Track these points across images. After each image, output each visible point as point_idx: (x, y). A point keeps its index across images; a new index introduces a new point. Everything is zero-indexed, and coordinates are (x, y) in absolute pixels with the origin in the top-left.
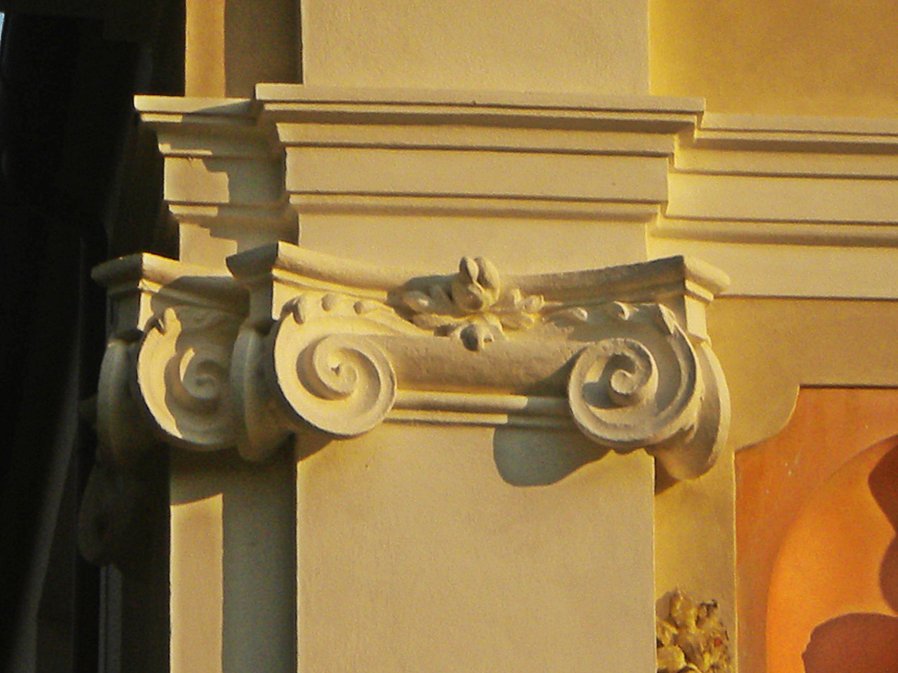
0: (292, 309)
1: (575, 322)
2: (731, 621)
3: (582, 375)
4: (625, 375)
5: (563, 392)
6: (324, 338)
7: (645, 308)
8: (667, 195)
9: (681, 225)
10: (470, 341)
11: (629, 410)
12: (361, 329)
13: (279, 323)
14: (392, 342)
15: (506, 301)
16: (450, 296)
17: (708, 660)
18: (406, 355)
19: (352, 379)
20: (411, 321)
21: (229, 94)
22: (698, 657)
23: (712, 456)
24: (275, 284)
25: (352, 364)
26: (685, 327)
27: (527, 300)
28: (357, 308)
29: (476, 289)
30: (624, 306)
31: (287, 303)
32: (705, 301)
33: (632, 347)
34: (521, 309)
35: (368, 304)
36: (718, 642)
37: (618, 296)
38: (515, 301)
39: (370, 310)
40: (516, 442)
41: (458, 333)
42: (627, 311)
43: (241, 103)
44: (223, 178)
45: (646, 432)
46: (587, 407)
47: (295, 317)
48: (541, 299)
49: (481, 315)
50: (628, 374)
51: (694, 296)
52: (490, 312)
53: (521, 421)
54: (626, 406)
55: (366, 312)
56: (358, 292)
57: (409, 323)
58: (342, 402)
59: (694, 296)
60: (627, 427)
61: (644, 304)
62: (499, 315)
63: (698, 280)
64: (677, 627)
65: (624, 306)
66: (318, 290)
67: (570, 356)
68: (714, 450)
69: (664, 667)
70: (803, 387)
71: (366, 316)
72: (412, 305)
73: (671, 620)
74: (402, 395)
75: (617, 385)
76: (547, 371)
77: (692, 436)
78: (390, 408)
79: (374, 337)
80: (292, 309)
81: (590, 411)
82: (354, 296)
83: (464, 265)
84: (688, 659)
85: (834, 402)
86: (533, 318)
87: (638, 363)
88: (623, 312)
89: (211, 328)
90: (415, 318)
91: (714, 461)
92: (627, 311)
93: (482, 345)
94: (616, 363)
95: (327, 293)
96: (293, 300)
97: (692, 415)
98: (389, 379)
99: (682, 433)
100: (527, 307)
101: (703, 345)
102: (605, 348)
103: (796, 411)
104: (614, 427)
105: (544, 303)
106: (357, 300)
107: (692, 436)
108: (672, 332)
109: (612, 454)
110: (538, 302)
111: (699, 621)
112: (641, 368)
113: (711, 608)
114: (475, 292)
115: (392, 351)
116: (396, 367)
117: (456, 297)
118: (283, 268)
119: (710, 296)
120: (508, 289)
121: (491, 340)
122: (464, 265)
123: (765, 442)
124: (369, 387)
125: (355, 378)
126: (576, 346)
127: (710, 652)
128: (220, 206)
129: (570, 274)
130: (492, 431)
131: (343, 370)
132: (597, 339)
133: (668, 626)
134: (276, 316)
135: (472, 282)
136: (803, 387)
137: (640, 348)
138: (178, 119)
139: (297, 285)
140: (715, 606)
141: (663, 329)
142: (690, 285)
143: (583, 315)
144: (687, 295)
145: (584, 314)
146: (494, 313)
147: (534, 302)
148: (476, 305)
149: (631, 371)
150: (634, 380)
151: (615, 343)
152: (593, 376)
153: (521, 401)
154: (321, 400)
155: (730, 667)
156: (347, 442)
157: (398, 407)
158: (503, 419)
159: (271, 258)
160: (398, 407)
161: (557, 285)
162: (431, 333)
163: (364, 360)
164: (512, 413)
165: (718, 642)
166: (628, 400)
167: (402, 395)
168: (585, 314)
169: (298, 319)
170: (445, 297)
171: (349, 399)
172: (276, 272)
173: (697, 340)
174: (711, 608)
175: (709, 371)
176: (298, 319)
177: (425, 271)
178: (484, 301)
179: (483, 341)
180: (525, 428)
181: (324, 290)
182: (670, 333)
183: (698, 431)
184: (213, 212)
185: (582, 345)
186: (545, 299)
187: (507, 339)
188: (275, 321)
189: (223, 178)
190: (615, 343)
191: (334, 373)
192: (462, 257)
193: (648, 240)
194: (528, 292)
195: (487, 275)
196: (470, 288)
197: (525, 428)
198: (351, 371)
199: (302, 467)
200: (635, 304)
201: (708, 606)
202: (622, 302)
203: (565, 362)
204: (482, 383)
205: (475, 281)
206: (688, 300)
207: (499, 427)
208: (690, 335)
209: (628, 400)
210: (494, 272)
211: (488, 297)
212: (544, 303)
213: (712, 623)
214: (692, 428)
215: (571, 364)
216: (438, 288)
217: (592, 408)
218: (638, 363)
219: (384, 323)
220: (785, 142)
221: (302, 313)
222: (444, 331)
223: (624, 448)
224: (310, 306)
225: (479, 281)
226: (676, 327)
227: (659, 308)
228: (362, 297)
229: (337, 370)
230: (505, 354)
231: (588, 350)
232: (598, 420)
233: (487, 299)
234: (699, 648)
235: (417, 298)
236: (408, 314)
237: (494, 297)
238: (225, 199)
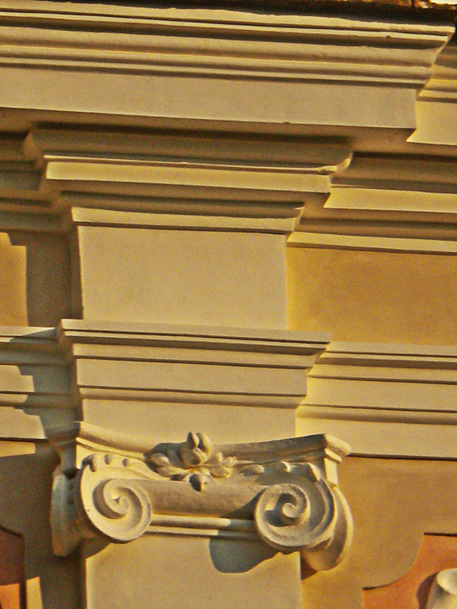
0: (88, 462)
1: (254, 473)
3: (264, 506)
5: (251, 517)
6: (108, 481)
8: (306, 390)
9: (312, 409)
11: (293, 527)
13: (81, 471)
14: (146, 483)
15: (213, 460)
20: (156, 472)
21: (32, 323)
25: (125, 497)
27: (225, 460)
28: (125, 463)
30: (287, 464)
31: (85, 459)
32: (338, 462)
33: (294, 489)
35: (131, 461)
41: (187, 479)
43: (49, 331)
44: (29, 379)
45: (305, 541)
46: (268, 526)
49: (198, 468)
50: (293, 506)
53: (224, 534)
55: (129, 466)
56: (126, 453)
57: (154, 473)
58: (118, 521)
60: (293, 538)
61: (299, 463)
62: (209, 468)
63: (334, 449)
65: (287, 464)
66: (104, 451)
72: (157, 462)
74: (156, 517)
76: (239, 505)
77: (329, 544)
78: (149, 524)
80: (88, 462)
83: (190, 437)
86: (229, 470)
87: (298, 498)
89: (314, 459)
90: (159, 469)
92: (289, 468)
93: (203, 487)
95: (108, 453)
96: (89, 457)
97: (330, 533)
99: (325, 543)
100: (227, 465)
101: (335, 488)
102: (277, 489)
104: (285, 537)
105: (236, 462)
106: (125, 458)
107: (329, 544)
109: (279, 555)
110: (233, 461)
114: (197, 453)
117: (184, 456)
119: (339, 459)
120: (216, 452)
122: (190, 437)
128: (29, 394)
130: (207, 542)
131: (121, 501)
132: (272, 484)
138: (7, 340)
141: (313, 479)
143: (260, 469)
145: (261, 469)
146: (205, 467)
148: (196, 461)
149: (295, 504)
152: (270, 507)
153: (226, 522)
154: (108, 519)
156: (126, 544)
157: (153, 524)
158: (215, 533)
159: (76, 432)
160: (153, 524)
162: (167, 479)
163: (130, 493)
164: (221, 529)
166: (292, 521)
167: (156, 517)
169: (93, 469)
171: (123, 519)
172: (78, 439)
173: (333, 485)
175: (340, 505)
176: (93, 469)
180: (227, 539)
181: (106, 452)
184: (23, 399)
187: (218, 484)
188: (78, 470)
189: (29, 379)
191: (115, 502)
192: (188, 432)
193: (299, 422)
194: (226, 455)
196: (194, 451)
197: (227, 539)
198: (125, 500)
199: (90, 562)
200: (294, 463)
206: (326, 460)
207: (212, 538)
209: (292, 521)
210: (208, 441)
211: (203, 456)
212: (236, 462)
214: (329, 539)
215: (255, 500)
216: (172, 452)
217: (271, 526)
218: (298, 498)
220: (133, 70)
221: (95, 464)
222: (176, 478)
223: (287, 550)
224: (99, 460)
225: (199, 447)
228: (128, 456)
229: (117, 500)
232: (275, 534)
233: (204, 458)
235: (159, 456)
236: (154, 467)
238: (32, 390)
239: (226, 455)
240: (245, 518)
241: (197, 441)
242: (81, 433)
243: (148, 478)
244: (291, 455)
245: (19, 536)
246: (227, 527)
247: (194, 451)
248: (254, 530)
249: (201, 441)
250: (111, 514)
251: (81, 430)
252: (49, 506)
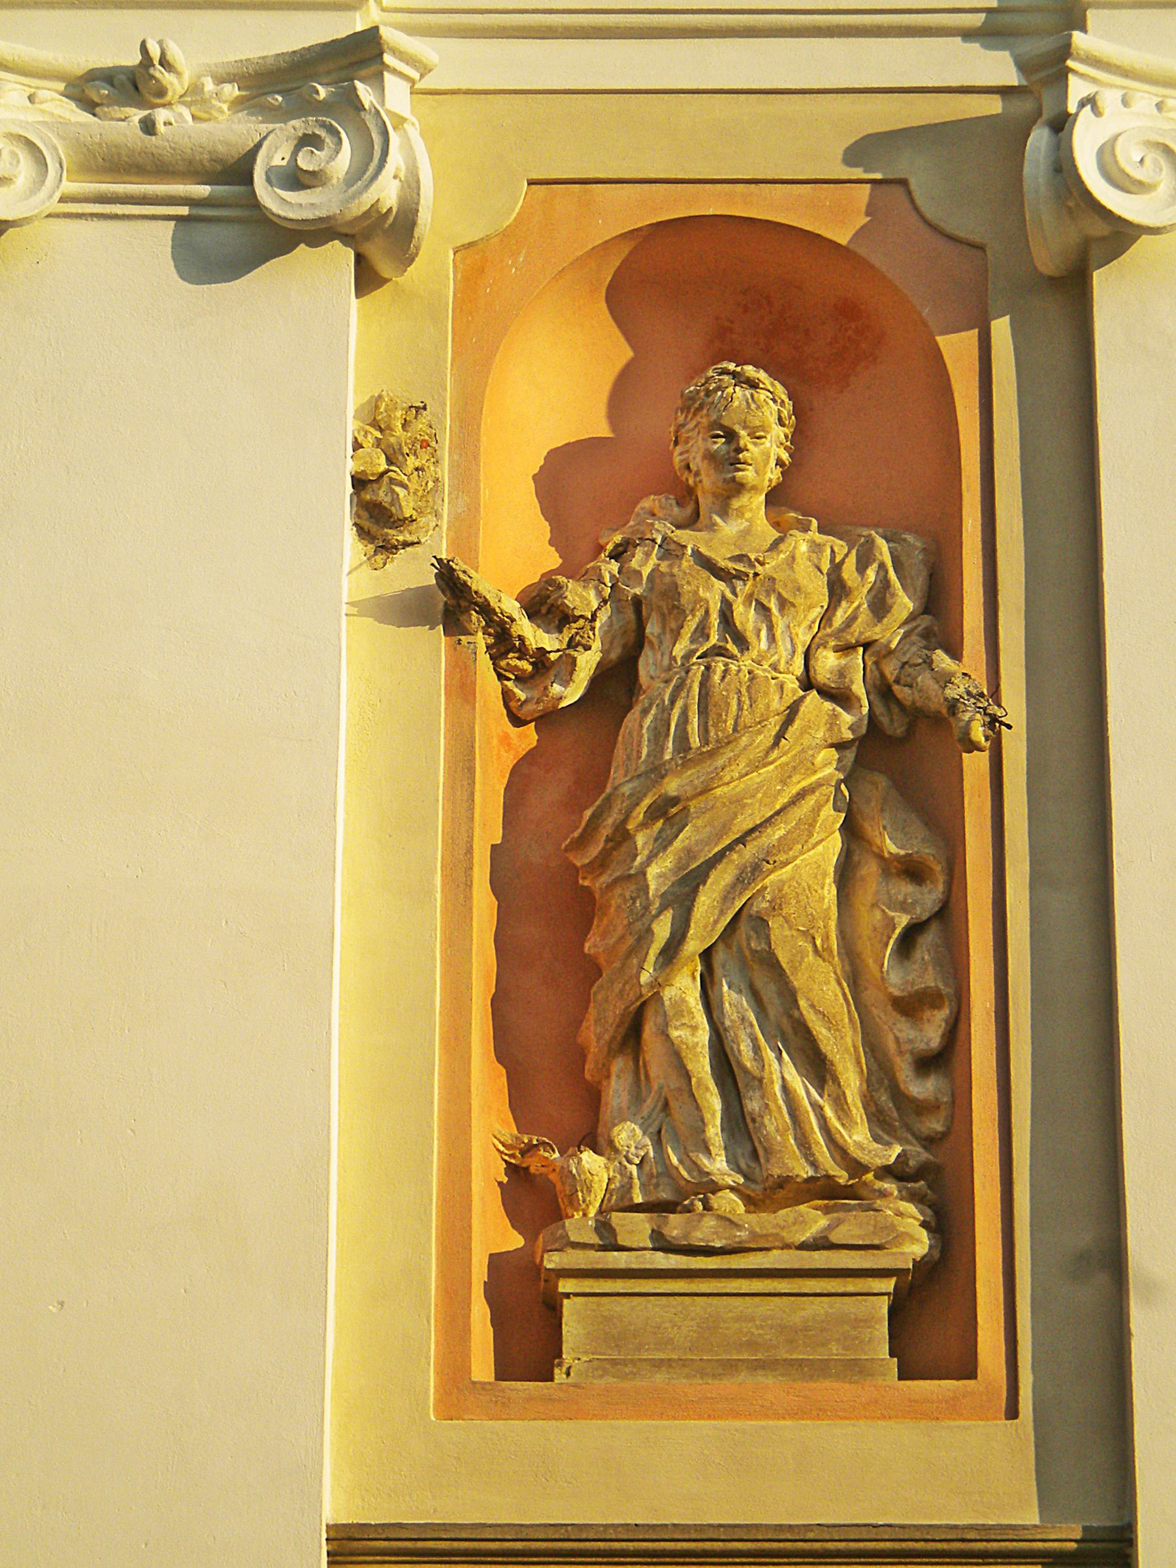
0: (1090, 101)
2: (441, 422)
3: (270, 157)
4: (312, 152)
5: (249, 181)
7: (342, 87)
10: (148, 127)
12: (31, 116)
14: (60, 126)
15: (195, 89)
16: (136, 88)
17: (412, 462)
18: (77, 139)
19: (15, 163)
22: (400, 458)
23: (414, 241)
24: (1070, 76)
26: (383, 103)
27: (219, 88)
29: (158, 72)
30: (319, 87)
33: (323, 125)
34: (211, 97)
35: (42, 94)
36: (425, 445)
37: (314, 77)
38: (206, 89)
39: (46, 101)
40: (207, 236)
42: (323, 92)
47: (1092, 107)
48: (233, 86)
51: (395, 72)
52: (179, 102)
53: (195, 211)
54: (314, 187)
56: (35, 82)
58: (1145, 197)
59: (395, 72)
62: (188, 105)
64: (381, 430)
65: (319, 87)
67: (258, 139)
68: (416, 235)
69: (362, 468)
70: (531, 183)
71: (43, 106)
73: (375, 424)
75: (304, 162)
77: (391, 218)
79: (44, 123)
81: (278, 195)
82: (30, 87)
84: (390, 461)
85: (566, 199)
87: (322, 133)
88: (317, 92)
90: (98, 110)
91: (418, 248)
92: (323, 92)
93: (161, 128)
94: (308, 141)
98: (58, 165)
103: (522, 207)
106: (33, 90)
107: (391, 218)
108: (367, 107)
111: (405, 425)
112: (331, 144)
113: (420, 409)
114: (158, 75)
115: (61, 138)
116: (68, 156)
118: (1075, 59)
121: (170, 124)
123: (486, 239)
124: (723, 1023)
125: (18, 162)
126: (264, 128)
127: (415, 454)
129: (309, 49)
131: (1147, 161)
133: (372, 430)
134: (1072, 108)
135: (153, 65)
136: (531, 183)
137: (331, 124)
139: (1094, 80)
140: (425, 408)
142: (387, 58)
144: (388, 71)
146: (184, 104)
147: (225, 89)
150: (323, 157)
151: (307, 122)
153: (203, 190)
155: (438, 469)
158: (184, 211)
159: (1066, 51)
160: (62, 200)
161: (251, 71)
163: (30, 145)
165: (425, 445)
168: (280, 99)
170: (132, 89)
172: (1070, 63)
173: (400, 121)
174: (420, 409)
177: (107, 60)
178: (168, 87)
179: (162, 124)
181: (1123, 88)
182: (365, 109)
183: (397, 213)
185: (271, 126)
186: (239, 89)
190: (307, 122)
194: (220, 80)
195: (169, 57)
196: (152, 71)
198: (1155, 161)
201: (417, 408)
202: (320, 84)
203: (252, 145)
204: (160, 169)
205: (156, 62)
207: (178, 219)
208: (388, 112)
210: (176, 53)
213: (420, 425)
215: (258, 146)
219: (61, 114)
221: (1099, 103)
224: (1109, 99)
225: (161, 64)
226: (371, 102)
227: (355, 89)
230: (186, 137)
231: (277, 131)
234: (400, 449)
236: (91, 106)
237: (181, 83)
239: (220, 80)
240: (245, 184)
241: (155, 52)
242: (1073, 50)
243: (65, 119)
244: (328, 73)
245: (981, 248)
246: (205, 199)
247: (152, 71)
248: (256, 205)
249: (163, 54)
250: (1128, 184)
251: (1073, 45)
252: (1020, 179)
